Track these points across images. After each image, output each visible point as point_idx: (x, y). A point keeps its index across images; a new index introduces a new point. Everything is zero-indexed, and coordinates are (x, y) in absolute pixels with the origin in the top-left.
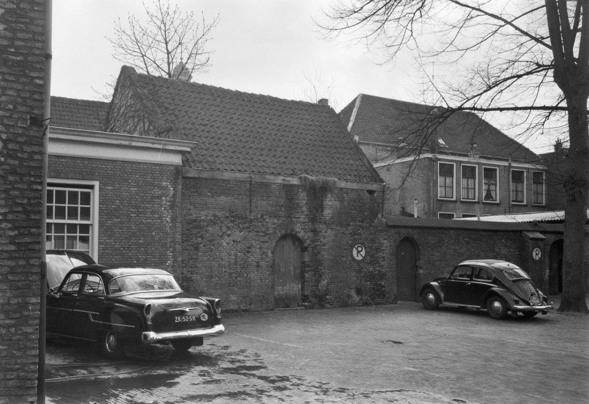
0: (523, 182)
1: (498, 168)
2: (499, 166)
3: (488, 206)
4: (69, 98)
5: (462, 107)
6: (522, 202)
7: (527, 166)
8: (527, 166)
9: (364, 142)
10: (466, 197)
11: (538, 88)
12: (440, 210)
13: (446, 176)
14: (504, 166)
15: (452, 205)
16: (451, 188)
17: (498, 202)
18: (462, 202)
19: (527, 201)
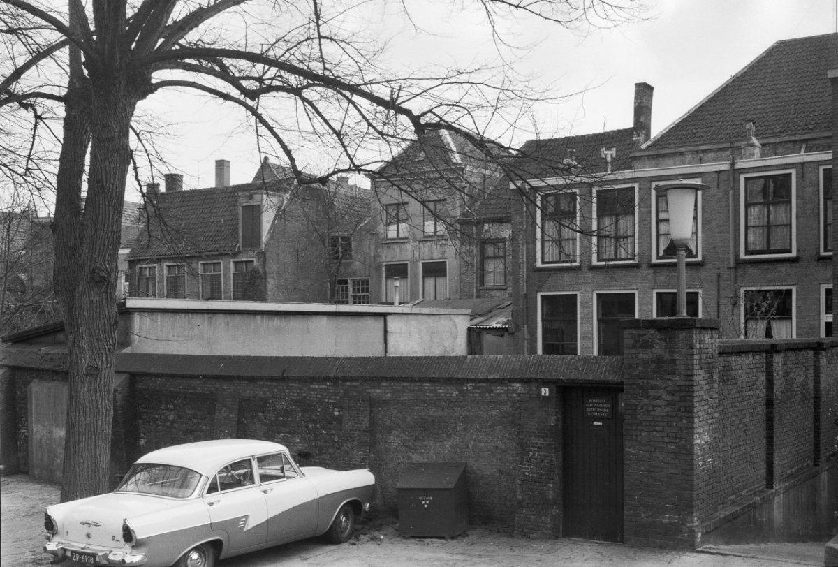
0: (634, 214)
1: (636, 186)
2: (634, 180)
3: (664, 271)
4: (591, 133)
5: (130, 130)
6: (789, 251)
7: (802, 157)
8: (802, 157)
9: (667, 151)
10: (558, 260)
11: (286, 38)
12: (540, 288)
13: (617, 215)
14: (719, 172)
15: (567, 278)
16: (248, 263)
17: (699, 259)
18: (593, 268)
19: (798, 250)
